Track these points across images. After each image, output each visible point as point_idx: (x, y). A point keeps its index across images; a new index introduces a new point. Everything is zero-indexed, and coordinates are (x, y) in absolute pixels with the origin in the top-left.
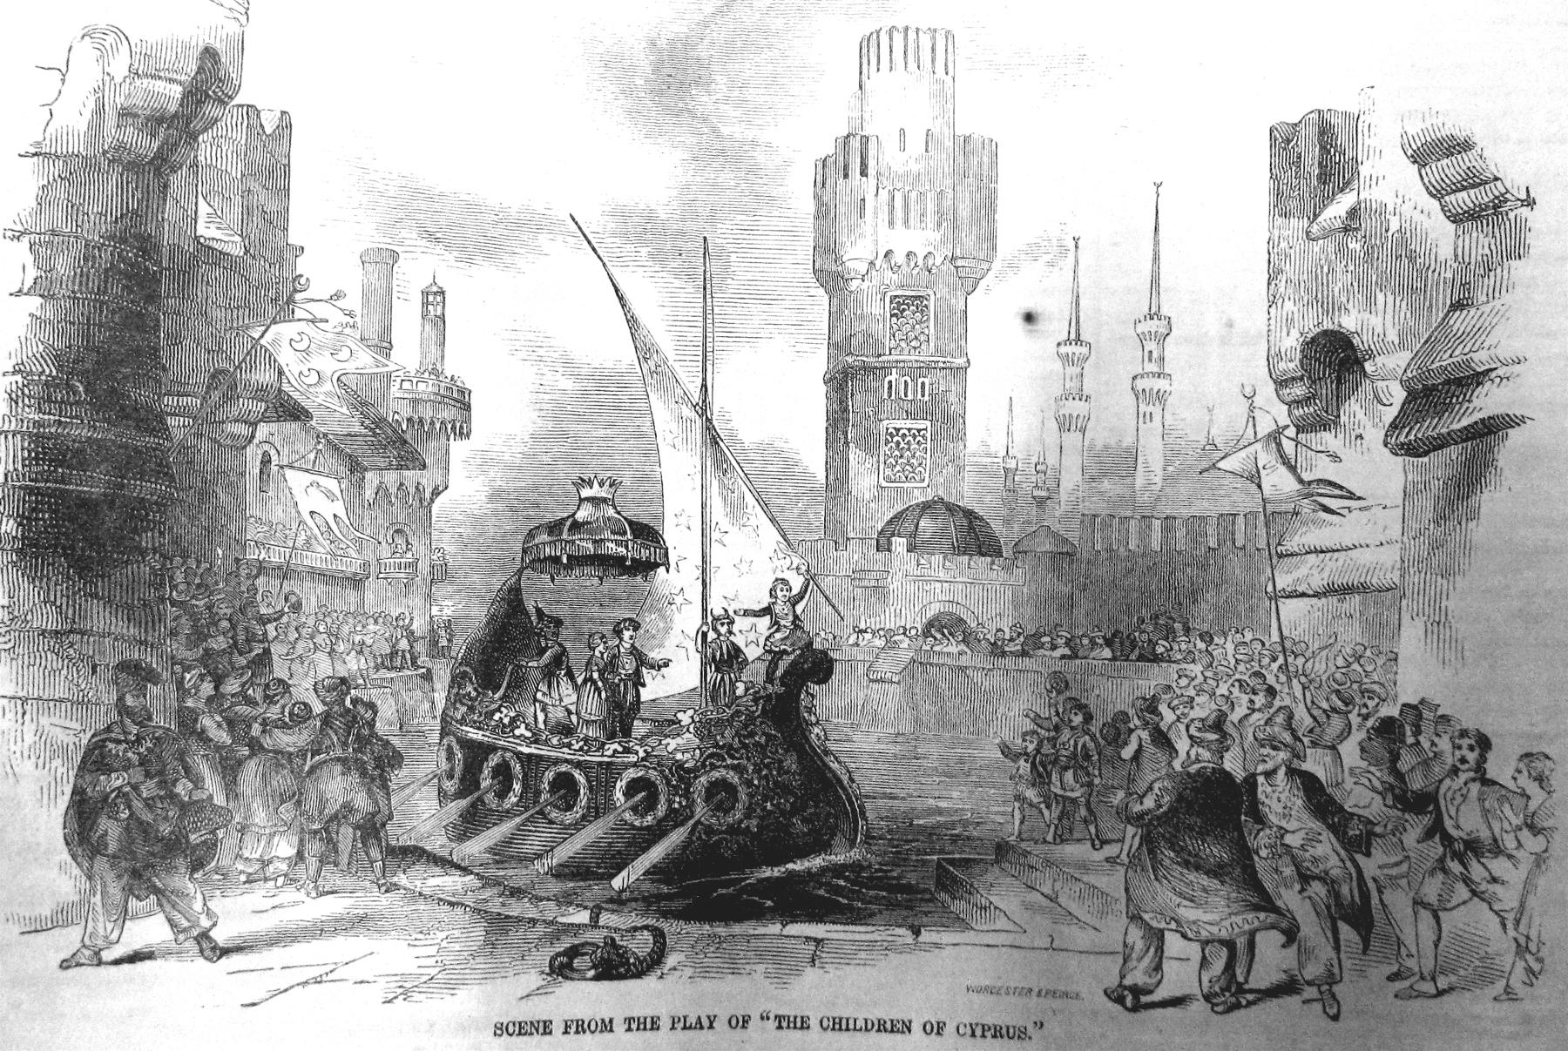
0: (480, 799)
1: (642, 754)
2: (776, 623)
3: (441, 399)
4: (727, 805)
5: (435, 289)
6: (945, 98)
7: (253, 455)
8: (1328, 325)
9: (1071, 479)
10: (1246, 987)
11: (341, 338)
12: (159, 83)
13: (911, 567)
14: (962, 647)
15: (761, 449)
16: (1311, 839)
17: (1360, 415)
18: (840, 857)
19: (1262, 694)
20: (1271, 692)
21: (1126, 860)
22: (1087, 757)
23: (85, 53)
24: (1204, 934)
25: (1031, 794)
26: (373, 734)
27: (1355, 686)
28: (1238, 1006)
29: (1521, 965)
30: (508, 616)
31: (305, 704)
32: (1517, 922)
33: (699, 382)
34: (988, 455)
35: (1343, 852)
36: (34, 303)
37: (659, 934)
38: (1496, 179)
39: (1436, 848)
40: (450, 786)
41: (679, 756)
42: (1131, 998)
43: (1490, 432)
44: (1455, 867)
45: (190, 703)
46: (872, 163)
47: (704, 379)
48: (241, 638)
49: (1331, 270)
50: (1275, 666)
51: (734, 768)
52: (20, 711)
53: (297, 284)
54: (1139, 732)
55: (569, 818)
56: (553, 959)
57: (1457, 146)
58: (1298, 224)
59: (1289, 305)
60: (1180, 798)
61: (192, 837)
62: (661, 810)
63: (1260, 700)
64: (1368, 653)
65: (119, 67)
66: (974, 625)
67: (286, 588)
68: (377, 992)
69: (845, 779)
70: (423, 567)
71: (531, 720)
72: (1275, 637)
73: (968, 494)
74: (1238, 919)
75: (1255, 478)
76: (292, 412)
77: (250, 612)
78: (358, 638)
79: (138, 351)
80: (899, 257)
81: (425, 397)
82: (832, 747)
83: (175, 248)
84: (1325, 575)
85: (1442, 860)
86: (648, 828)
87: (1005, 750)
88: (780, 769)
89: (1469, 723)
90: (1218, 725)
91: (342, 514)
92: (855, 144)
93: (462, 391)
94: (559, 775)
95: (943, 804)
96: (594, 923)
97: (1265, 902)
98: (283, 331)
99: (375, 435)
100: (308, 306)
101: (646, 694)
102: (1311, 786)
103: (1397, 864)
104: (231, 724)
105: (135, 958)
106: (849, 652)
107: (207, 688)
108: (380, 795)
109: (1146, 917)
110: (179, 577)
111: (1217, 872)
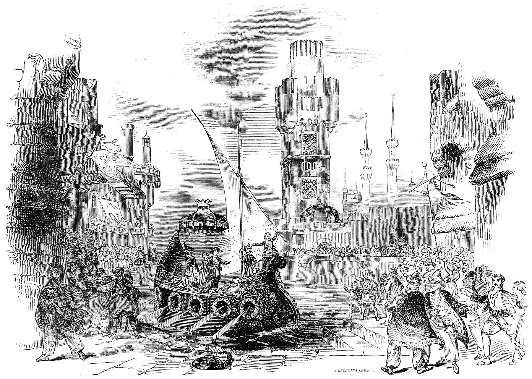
0: (168, 308)
1: (222, 293)
2: (266, 248)
3: (151, 175)
4: (251, 310)
5: (147, 137)
6: (320, 65)
7: (90, 194)
8: (450, 142)
9: (366, 195)
10: (428, 364)
11: (116, 155)
12: (53, 72)
13: (312, 227)
14: (330, 254)
15: (260, 188)
16: (448, 312)
17: (461, 171)
18: (291, 327)
19: (431, 266)
20: (434, 265)
21: (387, 324)
22: (374, 290)
23: (29, 63)
24: (414, 347)
25: (355, 303)
26: (132, 286)
27: (461, 262)
28: (426, 371)
29: (517, 352)
30: (175, 247)
31: (110, 277)
32: (516, 338)
33: (237, 166)
34: (337, 188)
35: (458, 317)
36: (18, 147)
37: (229, 355)
38: (502, 93)
39: (488, 314)
40: (158, 304)
41: (234, 294)
42: (391, 370)
43: (503, 177)
44: (495, 320)
45: (73, 276)
46: (295, 88)
47: (239, 165)
48: (88, 254)
49: (451, 124)
50: (435, 256)
51: (254, 298)
52: (21, 279)
53: (101, 137)
54: (390, 280)
55: (198, 314)
56: (194, 362)
57: (490, 83)
58: (440, 108)
59: (437, 136)
60: (405, 302)
61: (75, 320)
62: (229, 313)
63: (430, 268)
64: (465, 250)
65: (41, 68)
66: (334, 246)
67: (102, 239)
68: (136, 372)
69: (291, 301)
70: (147, 231)
71: (184, 282)
72: (435, 246)
73: (330, 201)
74: (424, 341)
75: (427, 194)
76: (103, 180)
77: (91, 246)
78: (126, 255)
79: (52, 162)
80: (305, 121)
81: (145, 174)
82: (286, 290)
83: (62, 127)
84: (451, 225)
85: (490, 318)
86: (224, 318)
87: (346, 289)
88: (269, 298)
89: (497, 273)
90: (417, 277)
91: (119, 214)
92: (289, 81)
93: (157, 171)
94: (194, 300)
95: (325, 308)
96: (207, 350)
97: (434, 335)
98: (98, 154)
99: (129, 187)
100: (106, 145)
101: (222, 273)
102: (447, 296)
103: (475, 320)
104: (86, 283)
105: (58, 359)
106: (291, 256)
107: (78, 272)
108: (135, 306)
109: (394, 342)
110: (68, 235)
111: (418, 326)
